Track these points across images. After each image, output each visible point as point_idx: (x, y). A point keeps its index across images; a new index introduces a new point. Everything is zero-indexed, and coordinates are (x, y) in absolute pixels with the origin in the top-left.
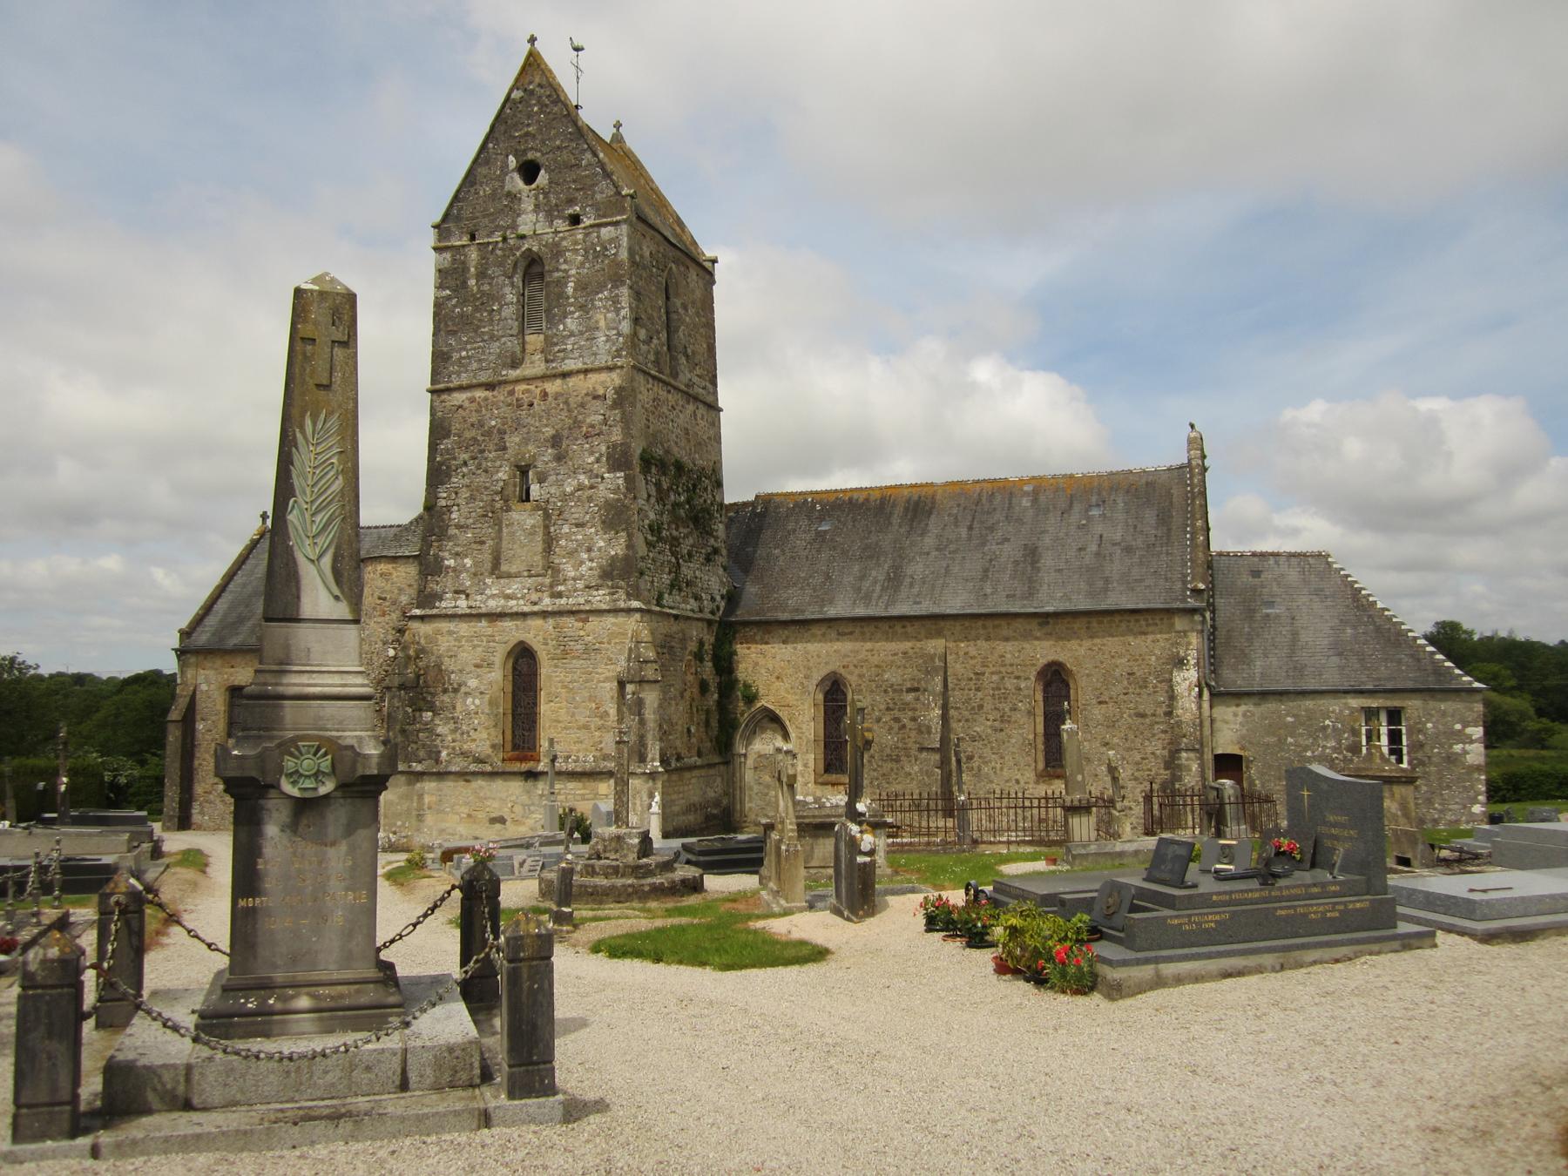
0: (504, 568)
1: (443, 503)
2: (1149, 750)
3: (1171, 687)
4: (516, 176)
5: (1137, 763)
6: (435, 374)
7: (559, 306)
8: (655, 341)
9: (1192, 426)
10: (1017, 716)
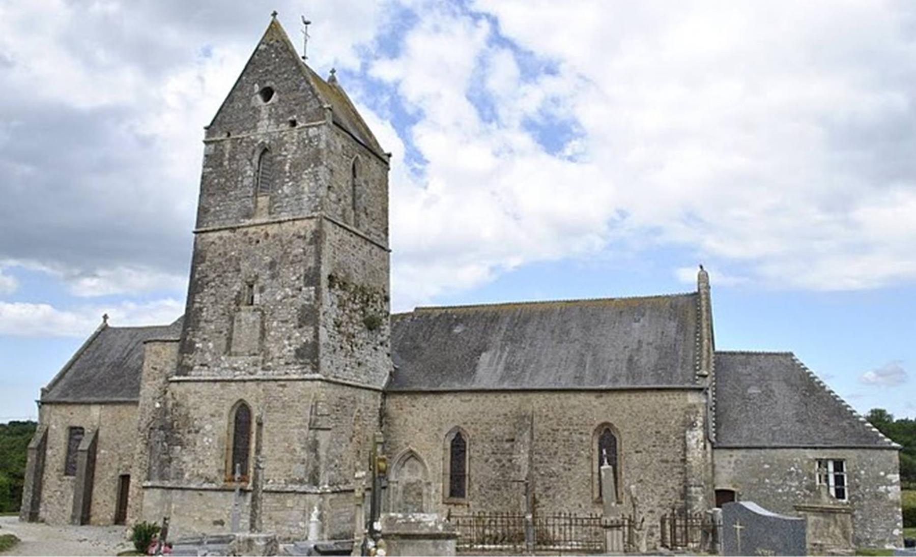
0: (233, 350)
1: (197, 305)
2: (671, 485)
3: (685, 442)
4: (258, 96)
5: (662, 495)
6: (199, 223)
7: (279, 178)
8: (342, 202)
9: (701, 267)
10: (579, 460)
